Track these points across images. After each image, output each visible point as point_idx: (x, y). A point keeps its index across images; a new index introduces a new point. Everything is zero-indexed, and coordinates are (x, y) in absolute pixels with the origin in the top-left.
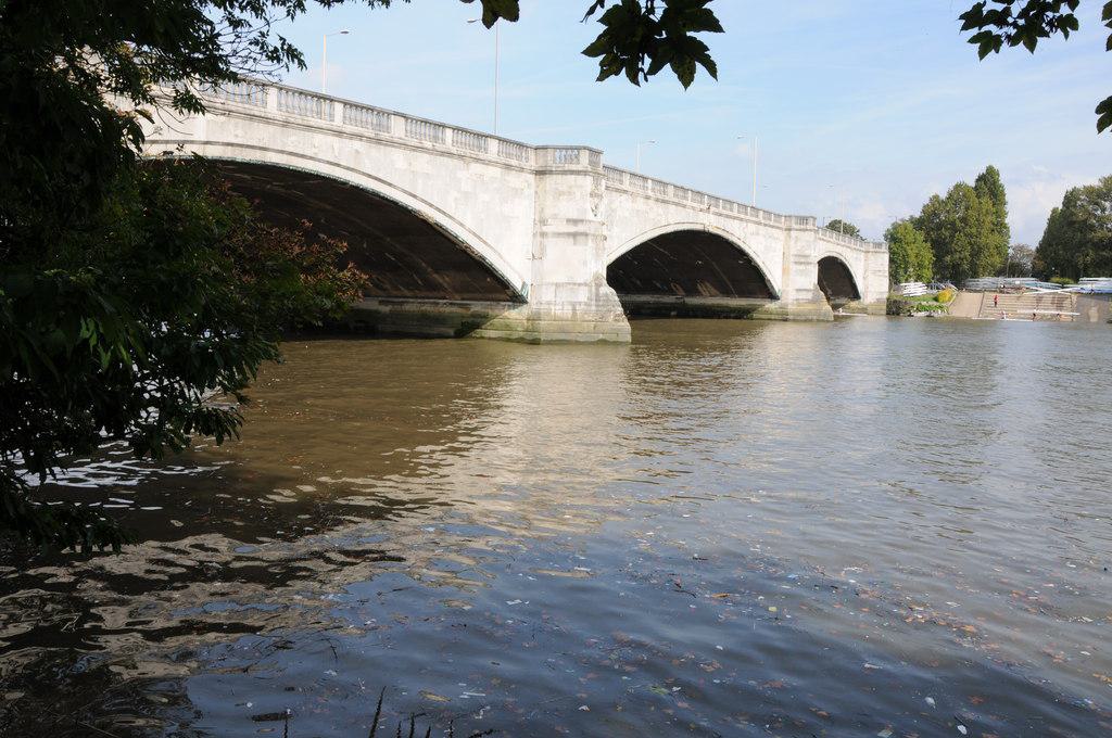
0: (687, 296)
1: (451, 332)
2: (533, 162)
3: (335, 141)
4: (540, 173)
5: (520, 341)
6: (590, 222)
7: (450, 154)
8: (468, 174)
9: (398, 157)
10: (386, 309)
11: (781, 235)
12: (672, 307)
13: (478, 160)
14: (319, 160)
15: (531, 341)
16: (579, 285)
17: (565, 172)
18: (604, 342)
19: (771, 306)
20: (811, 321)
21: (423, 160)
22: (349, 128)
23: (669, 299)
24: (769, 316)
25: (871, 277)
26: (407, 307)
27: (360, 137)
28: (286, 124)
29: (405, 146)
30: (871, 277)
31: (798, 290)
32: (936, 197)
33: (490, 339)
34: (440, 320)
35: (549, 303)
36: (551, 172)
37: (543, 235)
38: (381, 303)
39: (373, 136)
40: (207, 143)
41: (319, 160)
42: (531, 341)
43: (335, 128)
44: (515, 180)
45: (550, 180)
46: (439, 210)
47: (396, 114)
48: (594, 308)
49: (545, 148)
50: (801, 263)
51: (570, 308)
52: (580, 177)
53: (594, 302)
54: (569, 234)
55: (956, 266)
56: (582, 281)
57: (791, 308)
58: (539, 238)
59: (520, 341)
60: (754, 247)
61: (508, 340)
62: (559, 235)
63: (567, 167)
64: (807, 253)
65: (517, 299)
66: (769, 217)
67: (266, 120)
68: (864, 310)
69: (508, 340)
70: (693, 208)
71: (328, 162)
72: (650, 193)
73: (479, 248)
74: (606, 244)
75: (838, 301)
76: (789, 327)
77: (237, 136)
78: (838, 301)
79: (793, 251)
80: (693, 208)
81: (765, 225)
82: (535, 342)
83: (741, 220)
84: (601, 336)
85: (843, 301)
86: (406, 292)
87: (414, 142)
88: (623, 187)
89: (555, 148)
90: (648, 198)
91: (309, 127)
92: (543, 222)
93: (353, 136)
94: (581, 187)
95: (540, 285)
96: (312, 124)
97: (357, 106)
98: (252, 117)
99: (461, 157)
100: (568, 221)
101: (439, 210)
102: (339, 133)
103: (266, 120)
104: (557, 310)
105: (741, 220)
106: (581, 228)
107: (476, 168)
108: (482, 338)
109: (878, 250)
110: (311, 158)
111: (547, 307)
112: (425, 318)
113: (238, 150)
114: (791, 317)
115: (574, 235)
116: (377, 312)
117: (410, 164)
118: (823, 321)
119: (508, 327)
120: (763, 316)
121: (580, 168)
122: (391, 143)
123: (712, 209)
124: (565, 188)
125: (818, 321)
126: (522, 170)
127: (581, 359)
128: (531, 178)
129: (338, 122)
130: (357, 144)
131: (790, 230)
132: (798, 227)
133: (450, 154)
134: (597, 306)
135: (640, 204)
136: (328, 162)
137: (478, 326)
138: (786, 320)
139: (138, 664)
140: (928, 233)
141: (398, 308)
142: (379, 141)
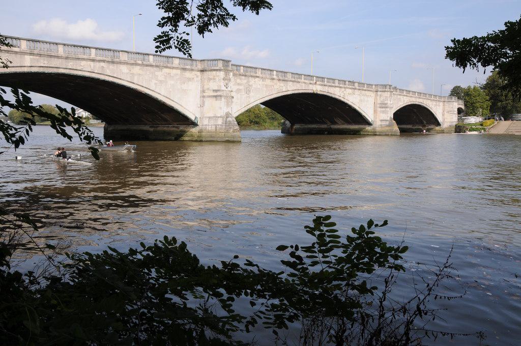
0: (332, 125)
1: (173, 138)
2: (200, 66)
3: (92, 64)
4: (202, 71)
5: (196, 141)
6: (223, 91)
7: (151, 66)
8: (161, 74)
9: (124, 69)
10: (152, 129)
11: (373, 94)
12: (326, 130)
13: (167, 67)
14: (84, 71)
15: (200, 141)
16: (219, 117)
17: (211, 70)
18: (228, 141)
19: (368, 128)
20: (388, 135)
21: (137, 69)
22: (99, 58)
23: (324, 126)
24: (368, 133)
25: (446, 115)
26: (159, 129)
27: (104, 61)
28: (67, 58)
29: (127, 63)
30: (446, 115)
31: (381, 120)
32: (457, 64)
33: (186, 141)
34: (169, 133)
35: (206, 125)
36: (206, 71)
37: (204, 97)
38: (151, 127)
39: (111, 60)
40: (31, 67)
41: (84, 71)
42: (200, 141)
43: (91, 58)
44: (188, 74)
45: (206, 74)
46: (147, 88)
47: (122, 51)
48: (224, 127)
49: (204, 60)
50: (383, 107)
51: (214, 127)
52: (218, 72)
53: (224, 124)
54: (214, 96)
55: (504, 108)
56: (219, 116)
57: (378, 129)
58: (202, 98)
59: (196, 141)
60: (153, 87)
61: (192, 141)
62: (209, 96)
63: (213, 68)
64: (386, 102)
65: (194, 124)
66: (362, 86)
67: (58, 57)
68: (442, 132)
69: (192, 141)
70: (305, 83)
71: (88, 72)
72: (275, 77)
73: (169, 103)
74: (233, 100)
75: (430, 127)
76: (377, 138)
77: (44, 64)
78: (430, 127)
79: (379, 102)
80: (305, 83)
81: (359, 90)
82: (201, 141)
83: (340, 87)
84: (227, 139)
85: (431, 127)
86: (158, 123)
87: (133, 62)
88: (257, 75)
89: (208, 60)
90: (273, 79)
91: (79, 59)
92: (204, 91)
93: (100, 61)
94: (219, 76)
95: (203, 118)
96: (80, 57)
97: (102, 50)
98: (51, 56)
99: (157, 66)
100: (213, 90)
101: (147, 88)
102: (93, 60)
103: (58, 57)
104: (209, 128)
105: (340, 87)
106: (218, 93)
107: (166, 70)
108: (184, 140)
109: (450, 100)
110: (80, 70)
111: (205, 127)
112: (164, 133)
113: (71, 70)
114: (378, 133)
115: (216, 96)
116: (149, 131)
117: (130, 71)
118: (394, 135)
119: (192, 136)
120: (366, 133)
121: (217, 68)
122: (120, 63)
123: (318, 83)
124: (212, 77)
125: (392, 135)
126: (192, 70)
127: (219, 147)
128: (199, 73)
129: (93, 56)
130: (102, 64)
131: (377, 91)
132: (381, 90)
133: (151, 66)
134: (226, 126)
135: (268, 82)
136: (88, 72)
137: (182, 135)
138: (375, 135)
139: (346, 237)
140: (489, 91)
141: (155, 129)
142: (113, 62)
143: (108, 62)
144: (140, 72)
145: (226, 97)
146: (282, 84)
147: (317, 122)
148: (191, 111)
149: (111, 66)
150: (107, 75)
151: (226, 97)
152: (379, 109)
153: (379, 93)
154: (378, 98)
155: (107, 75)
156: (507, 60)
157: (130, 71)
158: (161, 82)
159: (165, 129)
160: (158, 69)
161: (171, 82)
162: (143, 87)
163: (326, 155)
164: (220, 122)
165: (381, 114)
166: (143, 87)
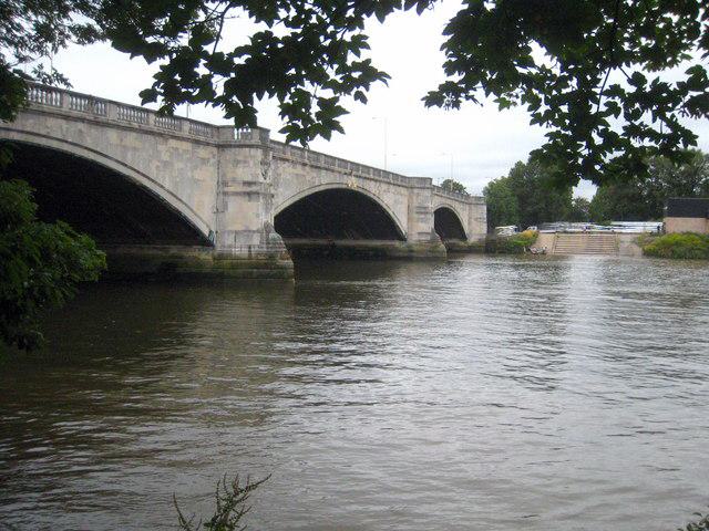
3: (64, 124)
16: (254, 232)
31: (419, 233)
35: (230, 246)
37: (225, 194)
54: (244, 193)
56: (255, 229)
64: (426, 205)
99: (161, 135)
104: (236, 251)
106: (254, 188)
110: (44, 136)
115: (249, 194)
117: (122, 140)
123: (354, 173)
128: (215, 150)
130: (80, 126)
143: (89, 122)
144: (138, 144)
145: (265, 195)
146: (314, 173)
147: (312, 236)
148: (205, 220)
149: (95, 131)
150: (86, 148)
151: (265, 195)
152: (416, 216)
153: (416, 191)
154: (415, 198)
155: (86, 148)
156: (293, 90)
157: (122, 140)
158: (166, 164)
159: (134, 251)
160: (162, 139)
161: (179, 165)
162: (138, 172)
163: (442, 281)
164: (256, 240)
165: (420, 224)
166: (138, 172)
